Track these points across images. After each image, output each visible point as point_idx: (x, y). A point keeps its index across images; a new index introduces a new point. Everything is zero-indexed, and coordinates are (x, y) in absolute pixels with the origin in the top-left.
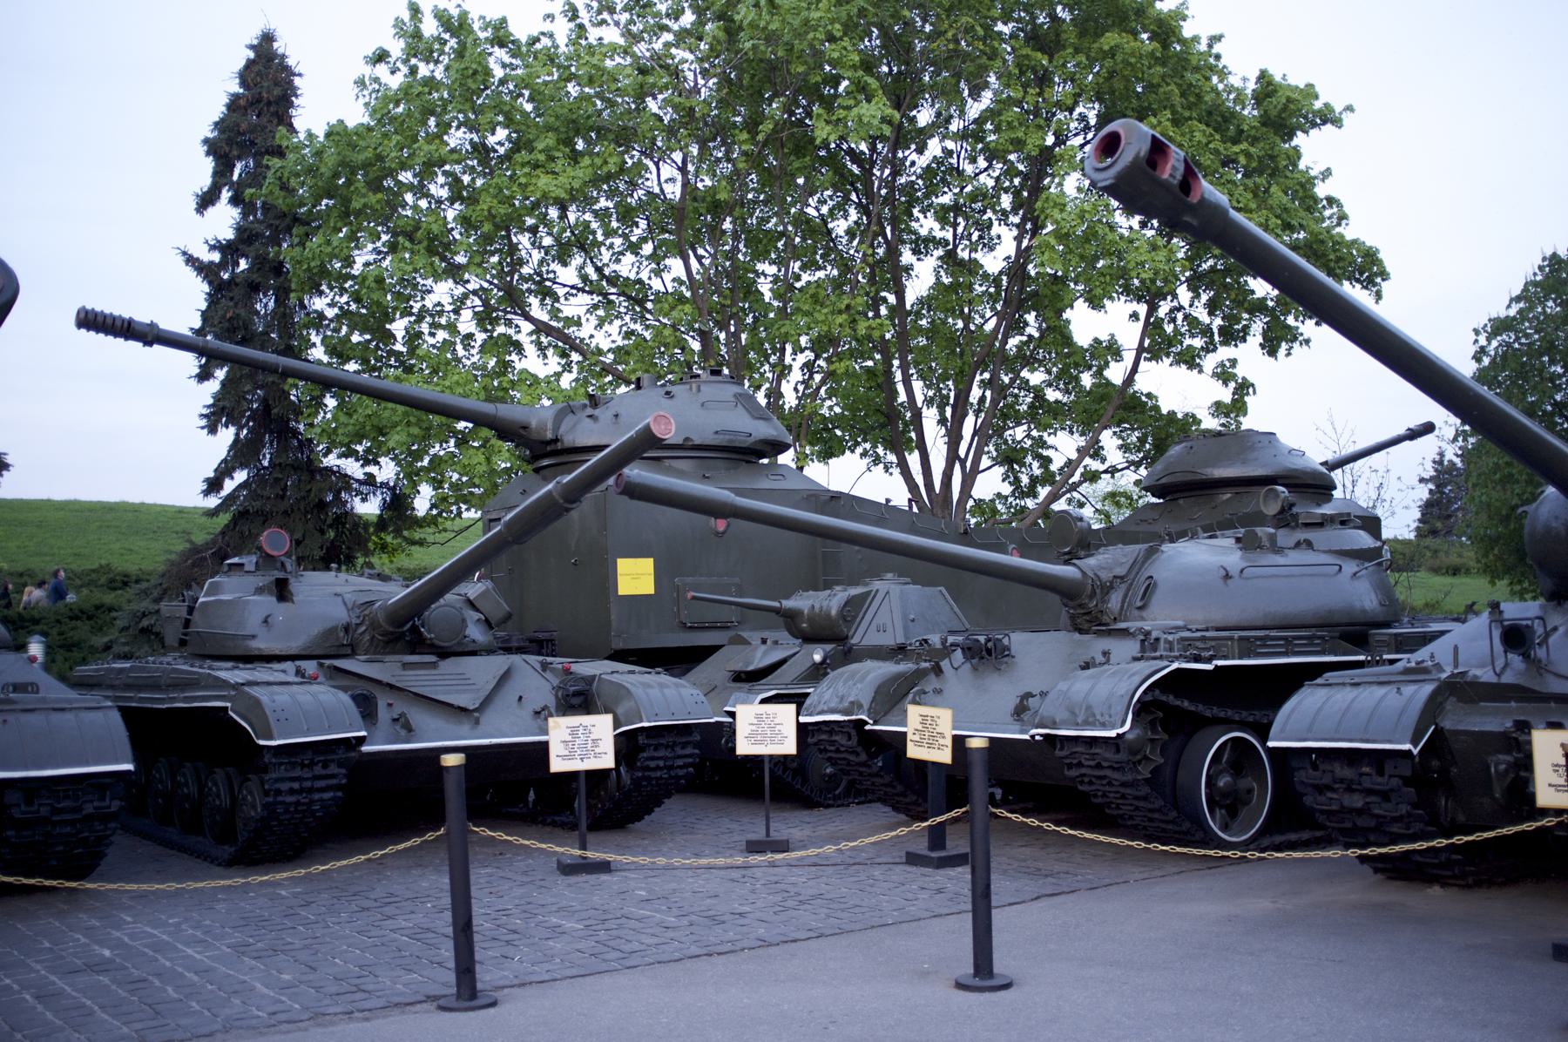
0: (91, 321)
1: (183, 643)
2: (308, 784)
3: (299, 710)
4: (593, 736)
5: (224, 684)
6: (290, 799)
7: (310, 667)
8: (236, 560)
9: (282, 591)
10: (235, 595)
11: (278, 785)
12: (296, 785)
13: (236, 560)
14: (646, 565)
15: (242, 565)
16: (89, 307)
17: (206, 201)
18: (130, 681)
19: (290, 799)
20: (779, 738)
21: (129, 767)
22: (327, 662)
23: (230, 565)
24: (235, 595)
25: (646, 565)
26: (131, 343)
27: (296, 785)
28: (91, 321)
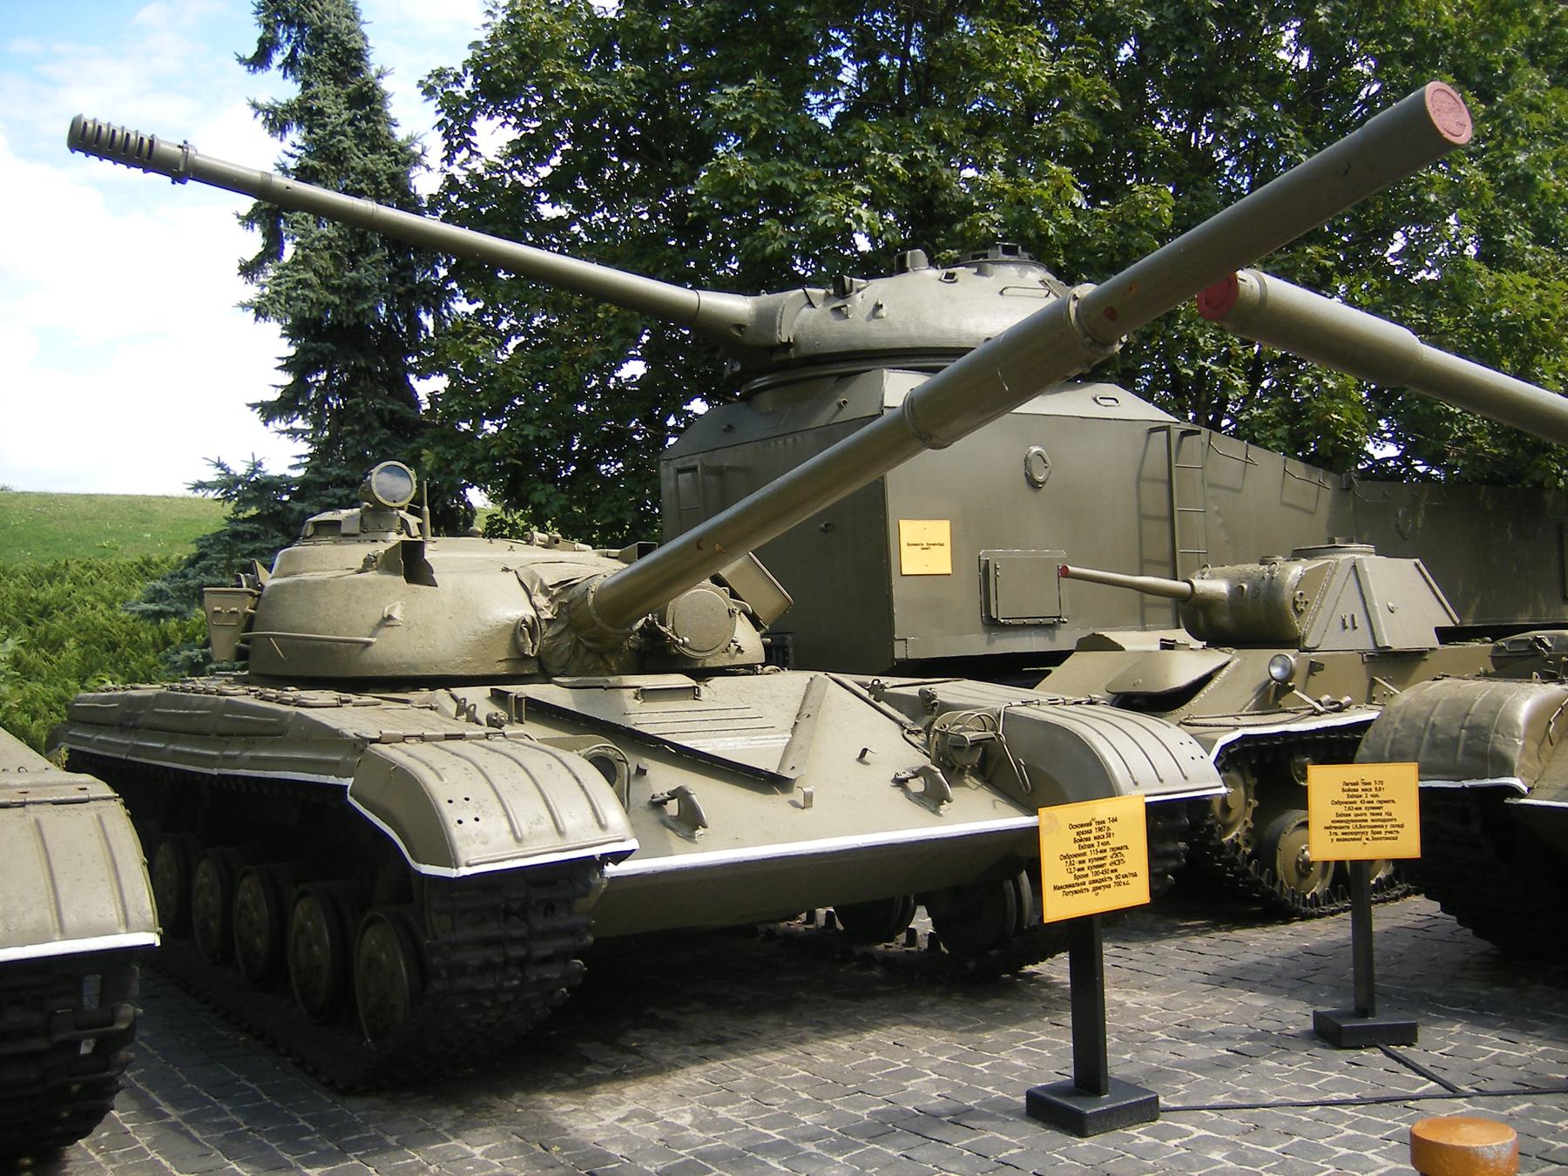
0: (89, 140)
1: (242, 655)
2: (516, 952)
3: (511, 806)
4: (1114, 842)
5: (332, 737)
6: (486, 983)
7: (478, 696)
8: (327, 516)
9: (411, 565)
10: (331, 577)
11: (459, 957)
12: (494, 955)
13: (327, 516)
14: (940, 530)
15: (337, 523)
16: (88, 117)
17: (260, 60)
18: (156, 720)
19: (486, 983)
20: (1385, 827)
21: (153, 939)
22: (515, 690)
23: (316, 524)
24: (331, 577)
25: (940, 530)
26: (153, 176)
27: (494, 955)
28: (89, 140)
